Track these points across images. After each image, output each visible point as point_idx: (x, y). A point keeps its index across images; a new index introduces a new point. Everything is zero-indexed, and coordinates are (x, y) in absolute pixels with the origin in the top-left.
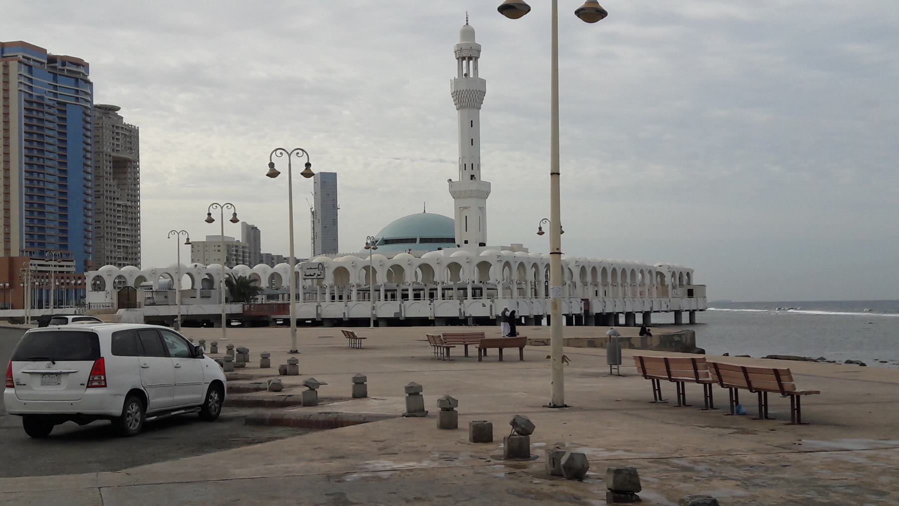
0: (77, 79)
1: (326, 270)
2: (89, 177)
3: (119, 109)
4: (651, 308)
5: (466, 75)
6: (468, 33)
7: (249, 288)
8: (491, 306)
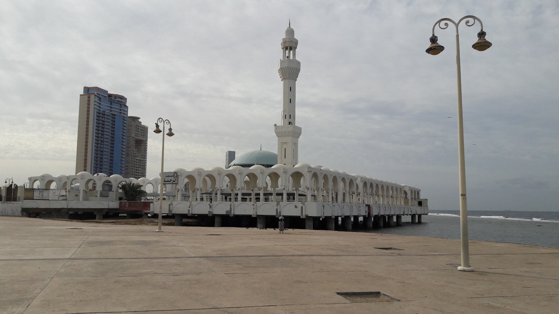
0: (121, 105)
1: (180, 178)
2: (124, 147)
3: (139, 118)
4: (404, 212)
5: (288, 57)
6: (290, 32)
7: (135, 191)
8: (302, 208)
